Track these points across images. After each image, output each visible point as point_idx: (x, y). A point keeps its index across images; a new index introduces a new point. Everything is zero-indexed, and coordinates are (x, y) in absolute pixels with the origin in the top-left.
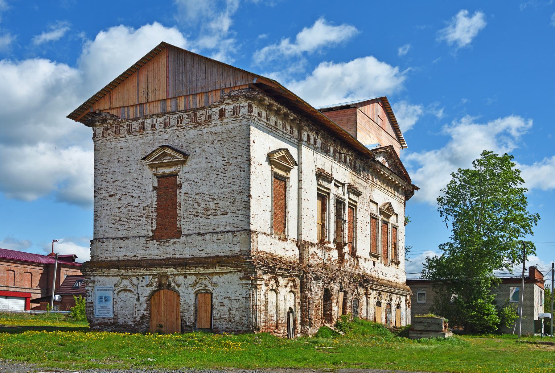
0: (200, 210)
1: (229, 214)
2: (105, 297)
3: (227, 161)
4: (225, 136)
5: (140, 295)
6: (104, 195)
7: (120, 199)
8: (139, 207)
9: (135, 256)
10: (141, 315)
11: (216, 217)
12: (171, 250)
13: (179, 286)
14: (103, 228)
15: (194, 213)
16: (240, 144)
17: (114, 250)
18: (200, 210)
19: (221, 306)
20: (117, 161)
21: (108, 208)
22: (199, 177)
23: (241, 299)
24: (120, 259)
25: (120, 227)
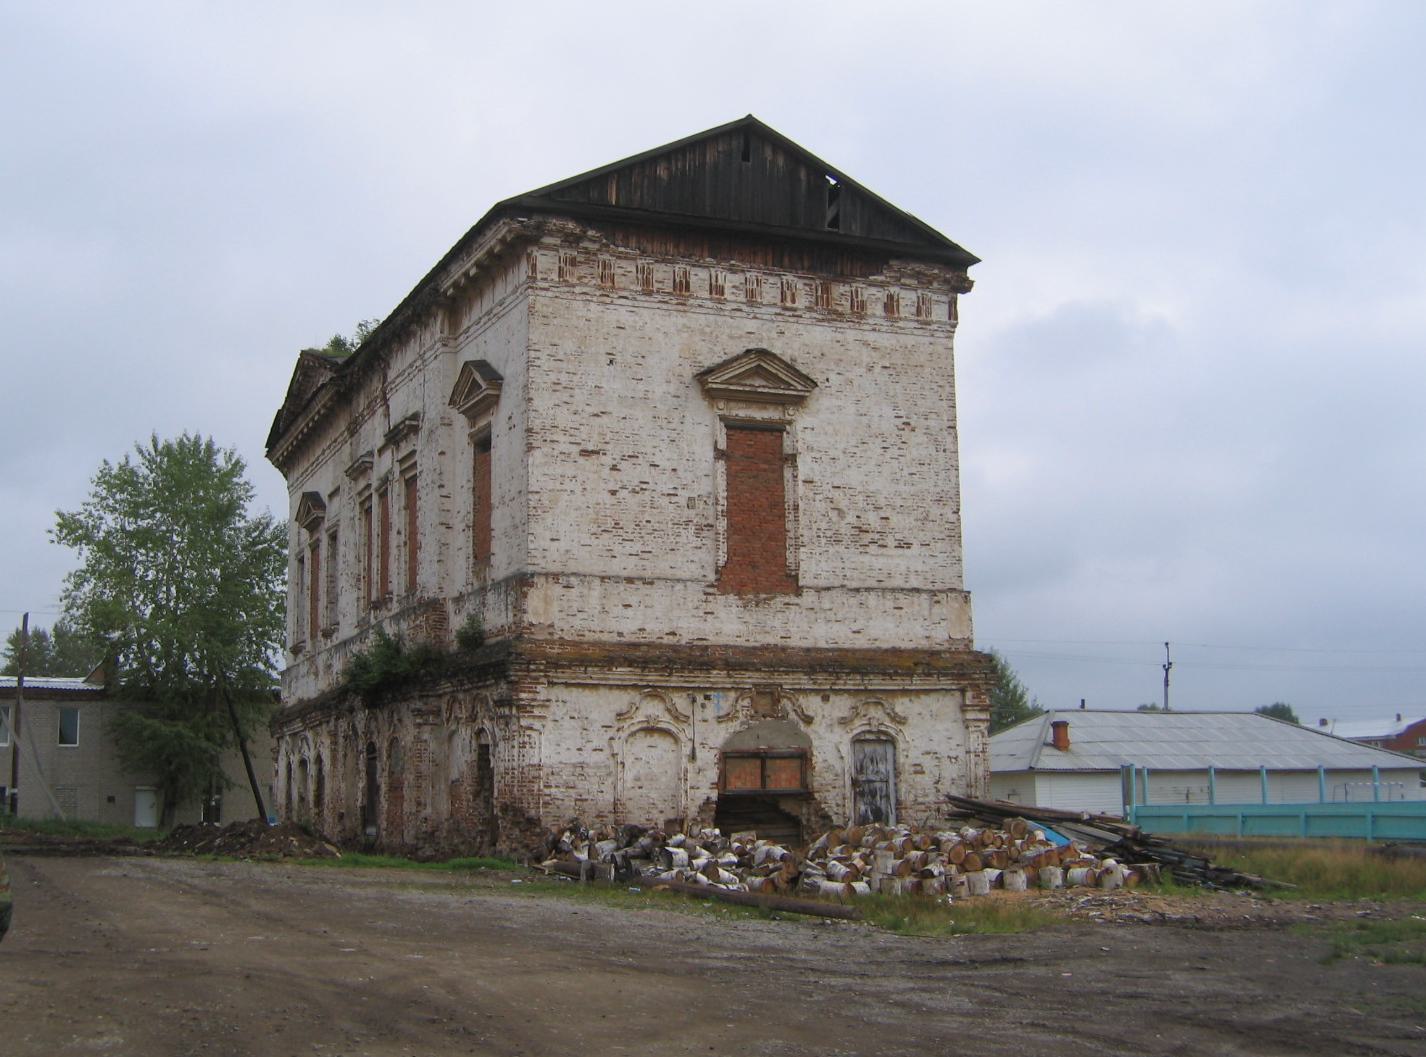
0: (845, 529)
3: (904, 420)
4: (897, 359)
5: (697, 745)
7: (614, 468)
8: (674, 499)
9: (673, 634)
10: (700, 802)
11: (884, 550)
12: (777, 623)
13: (809, 720)
14: (563, 545)
15: (829, 533)
17: (604, 611)
18: (845, 529)
19: (916, 772)
20: (605, 359)
21: (578, 490)
22: (841, 446)
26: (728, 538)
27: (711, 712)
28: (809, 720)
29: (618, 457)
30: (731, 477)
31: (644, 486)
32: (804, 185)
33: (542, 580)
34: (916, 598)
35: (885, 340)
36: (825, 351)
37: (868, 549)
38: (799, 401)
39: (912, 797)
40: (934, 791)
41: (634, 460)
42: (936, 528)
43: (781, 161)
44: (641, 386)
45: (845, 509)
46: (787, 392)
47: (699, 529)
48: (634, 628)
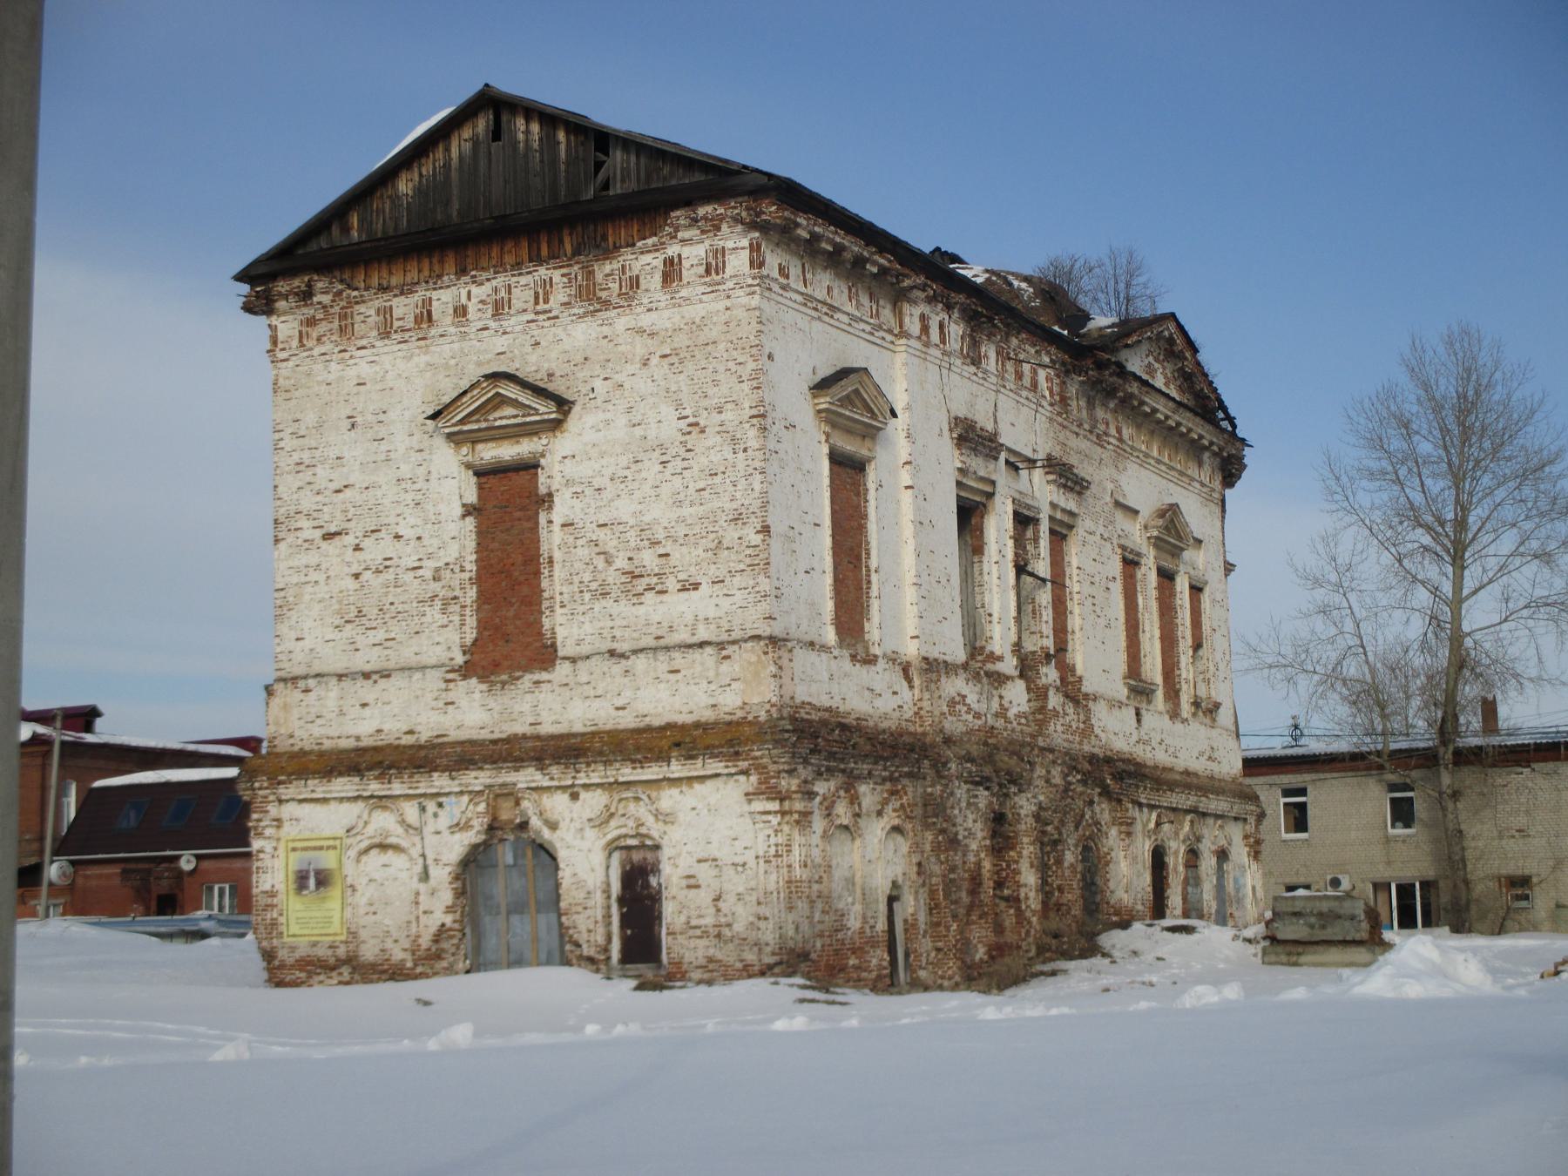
0: (612, 577)
1: (703, 587)
2: (318, 873)
3: (691, 420)
4: (682, 340)
5: (429, 862)
6: (308, 534)
7: (357, 548)
8: (420, 572)
10: (433, 929)
12: (526, 707)
13: (553, 826)
14: (307, 644)
15: (594, 586)
16: (731, 365)
17: (342, 713)
18: (612, 577)
19: (689, 887)
20: (347, 424)
22: (608, 472)
23: (752, 863)
24: (362, 744)
25: (359, 639)
26: (478, 610)
27: (444, 821)
28: (553, 826)
29: (360, 534)
30: (482, 534)
31: (388, 563)
32: (563, 147)
33: (282, 685)
34: (696, 655)
35: (663, 319)
36: (588, 354)
37: (643, 599)
38: (556, 425)
39: (683, 919)
40: (713, 910)
41: (376, 535)
42: (733, 557)
43: (535, 128)
44: (384, 446)
45: (612, 551)
46: (528, 419)
47: (445, 604)
48: (371, 730)
